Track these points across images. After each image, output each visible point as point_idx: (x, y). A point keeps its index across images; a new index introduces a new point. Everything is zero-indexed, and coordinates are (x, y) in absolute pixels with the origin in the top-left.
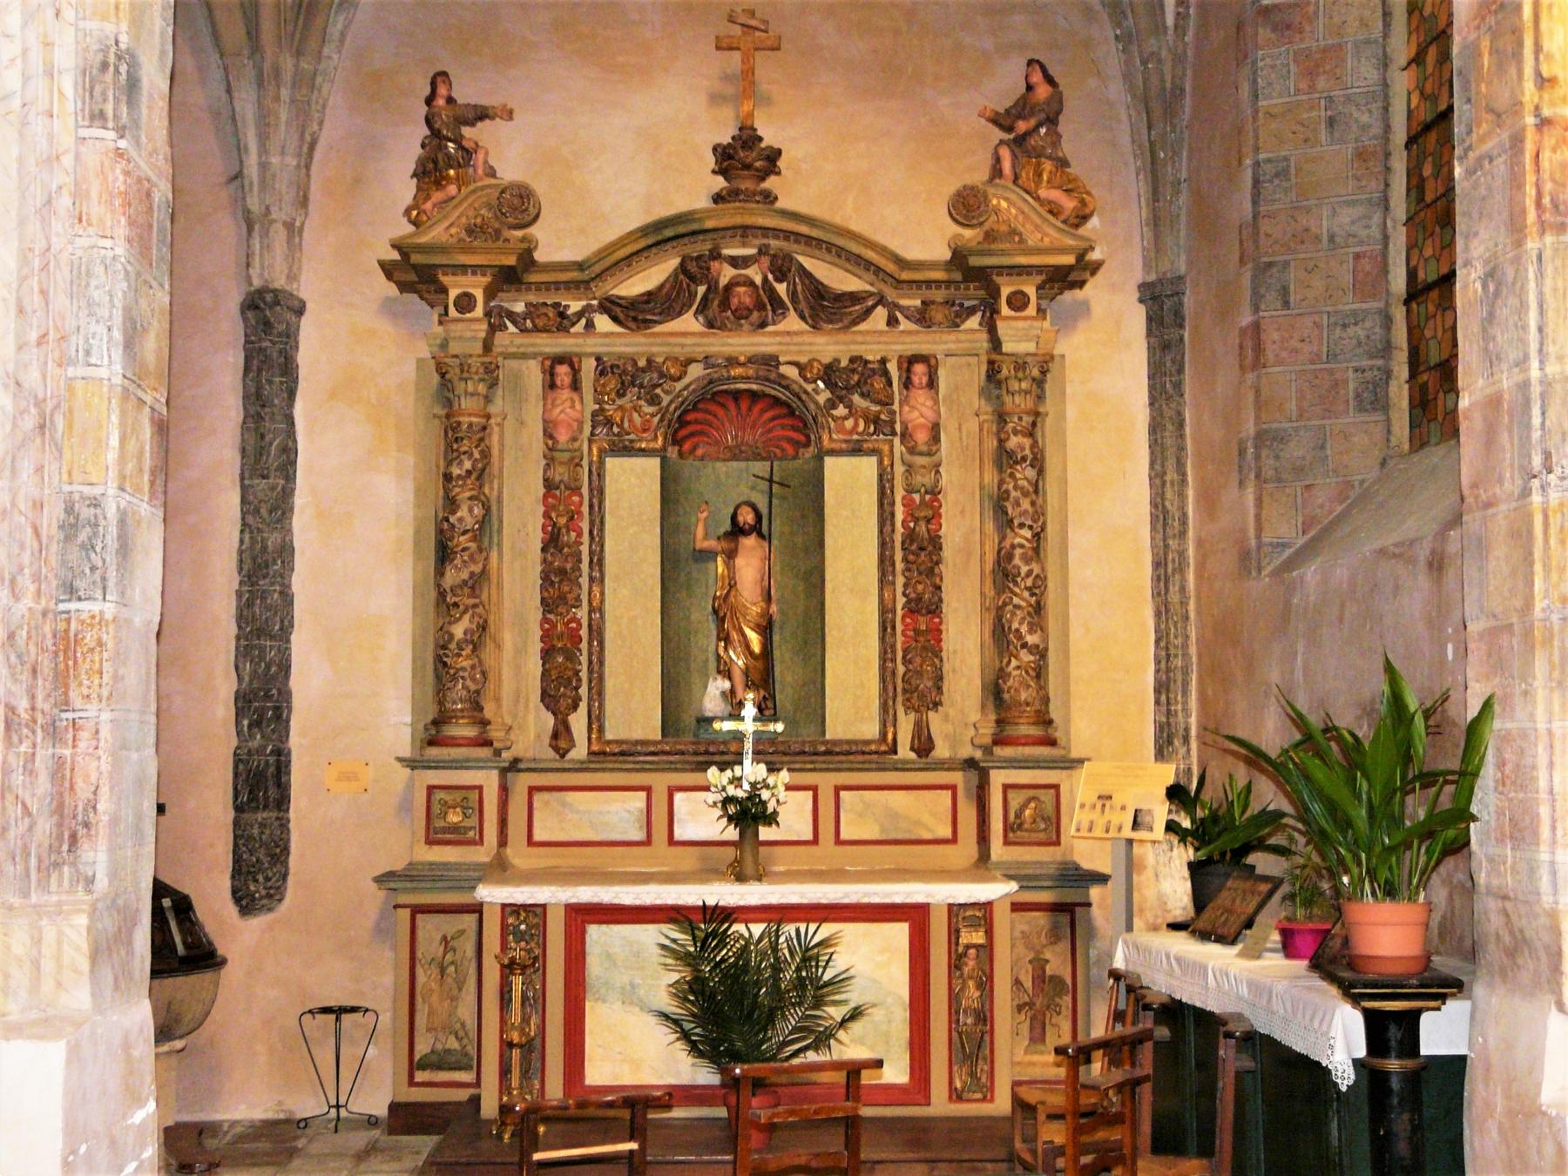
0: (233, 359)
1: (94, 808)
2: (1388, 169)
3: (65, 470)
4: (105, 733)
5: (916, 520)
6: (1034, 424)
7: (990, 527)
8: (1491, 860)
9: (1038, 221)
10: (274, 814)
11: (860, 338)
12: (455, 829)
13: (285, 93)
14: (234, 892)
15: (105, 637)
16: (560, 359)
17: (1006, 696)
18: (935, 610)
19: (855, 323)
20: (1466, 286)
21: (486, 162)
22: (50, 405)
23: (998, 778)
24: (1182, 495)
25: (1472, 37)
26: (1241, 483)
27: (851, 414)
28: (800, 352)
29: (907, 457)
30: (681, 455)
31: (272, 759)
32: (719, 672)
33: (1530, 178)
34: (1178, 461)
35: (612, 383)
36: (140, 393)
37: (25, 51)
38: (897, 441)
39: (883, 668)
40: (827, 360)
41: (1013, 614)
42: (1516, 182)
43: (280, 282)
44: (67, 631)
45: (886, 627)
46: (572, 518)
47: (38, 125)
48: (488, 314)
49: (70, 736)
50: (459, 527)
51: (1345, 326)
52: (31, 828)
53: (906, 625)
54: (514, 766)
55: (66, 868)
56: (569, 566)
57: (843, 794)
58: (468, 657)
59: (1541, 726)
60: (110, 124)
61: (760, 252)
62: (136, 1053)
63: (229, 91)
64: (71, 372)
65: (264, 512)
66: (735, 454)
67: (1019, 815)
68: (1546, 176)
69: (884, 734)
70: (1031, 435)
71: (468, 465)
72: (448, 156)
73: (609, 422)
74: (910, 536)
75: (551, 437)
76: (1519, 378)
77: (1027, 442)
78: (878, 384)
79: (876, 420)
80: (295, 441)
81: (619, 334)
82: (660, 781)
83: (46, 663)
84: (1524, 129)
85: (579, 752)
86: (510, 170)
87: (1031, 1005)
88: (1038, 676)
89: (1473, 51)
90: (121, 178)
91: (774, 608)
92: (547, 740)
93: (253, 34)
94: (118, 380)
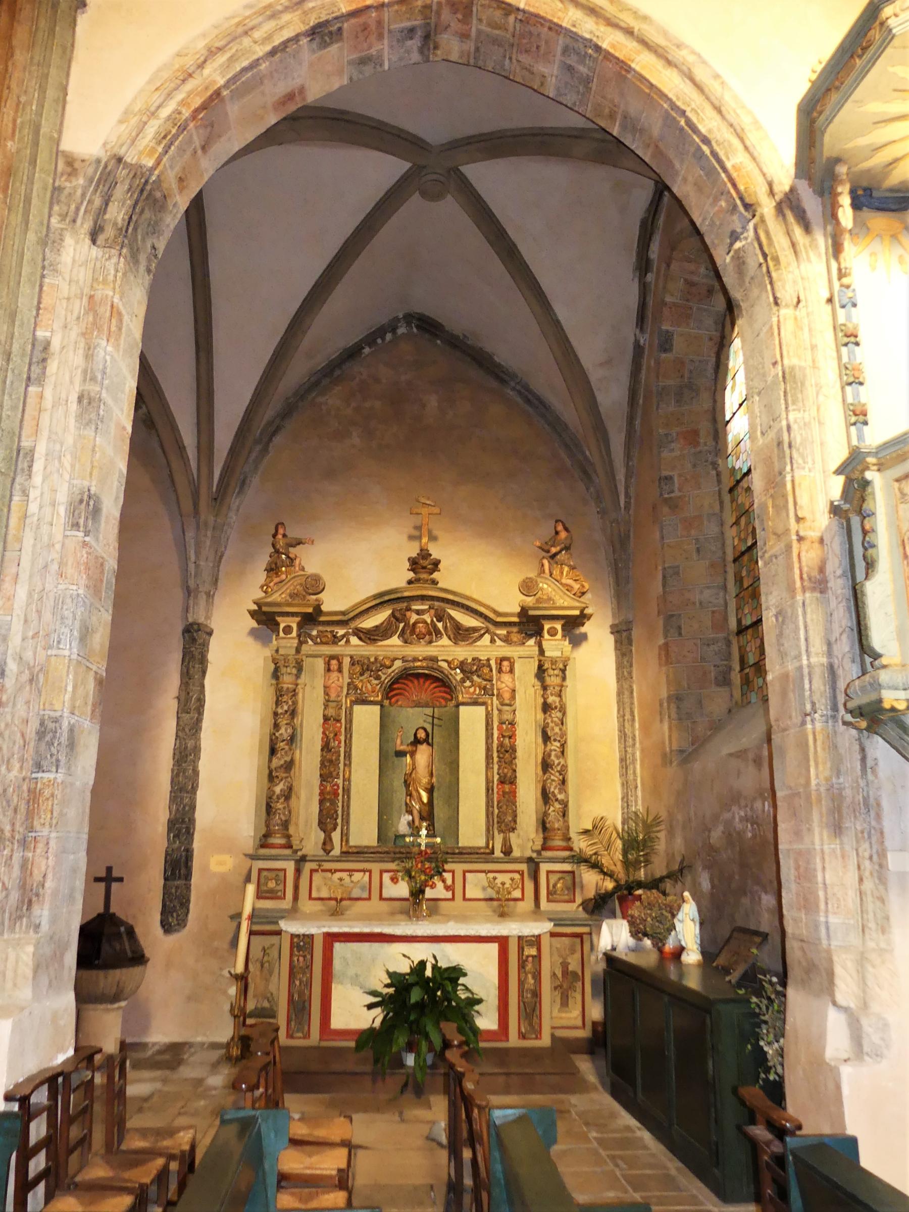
0: (177, 656)
1: (43, 886)
2: (725, 572)
3: (41, 704)
4: (53, 844)
5: (504, 737)
6: (561, 691)
7: (540, 740)
8: (795, 920)
9: (561, 594)
10: (184, 882)
11: (477, 649)
12: (271, 891)
13: (209, 533)
14: (161, 922)
15: (56, 792)
16: (332, 657)
17: (548, 825)
18: (513, 782)
19: (475, 641)
20: (767, 619)
21: (300, 564)
22: (37, 669)
23: (544, 868)
24: (633, 726)
25: (763, 499)
26: (661, 721)
27: (473, 685)
28: (448, 655)
29: (500, 707)
30: (390, 703)
31: (184, 854)
32: (407, 811)
33: (796, 565)
34: (631, 709)
35: (358, 669)
36: (88, 664)
37: (42, 494)
38: (495, 698)
39: (487, 810)
40: (461, 659)
41: (551, 784)
42: (790, 568)
43: (201, 620)
44: (35, 788)
45: (489, 790)
46: (336, 735)
47: (45, 529)
48: (299, 636)
49: (32, 846)
50: (280, 739)
51: (708, 645)
52: (7, 896)
53: (499, 789)
54: (303, 859)
55: (25, 920)
56: (334, 758)
57: (467, 875)
58: (282, 803)
59: (818, 847)
60: (81, 529)
61: (430, 608)
62: (62, 1023)
63: (184, 533)
64: (49, 652)
65: (187, 730)
66: (418, 705)
67: (555, 886)
68: (804, 564)
69: (488, 844)
70: (560, 696)
71: (286, 708)
72: (283, 561)
73: (356, 688)
74: (501, 745)
75: (328, 694)
76: (797, 664)
77: (557, 699)
78: (486, 670)
79: (485, 688)
80: (204, 696)
81: (362, 646)
82: (375, 867)
83: (23, 806)
84: (791, 542)
85: (336, 851)
86: (311, 570)
87: (561, 986)
88: (564, 815)
89: (764, 506)
90: (85, 556)
91: (434, 780)
92: (320, 845)
93: (196, 505)
94: (74, 657)
